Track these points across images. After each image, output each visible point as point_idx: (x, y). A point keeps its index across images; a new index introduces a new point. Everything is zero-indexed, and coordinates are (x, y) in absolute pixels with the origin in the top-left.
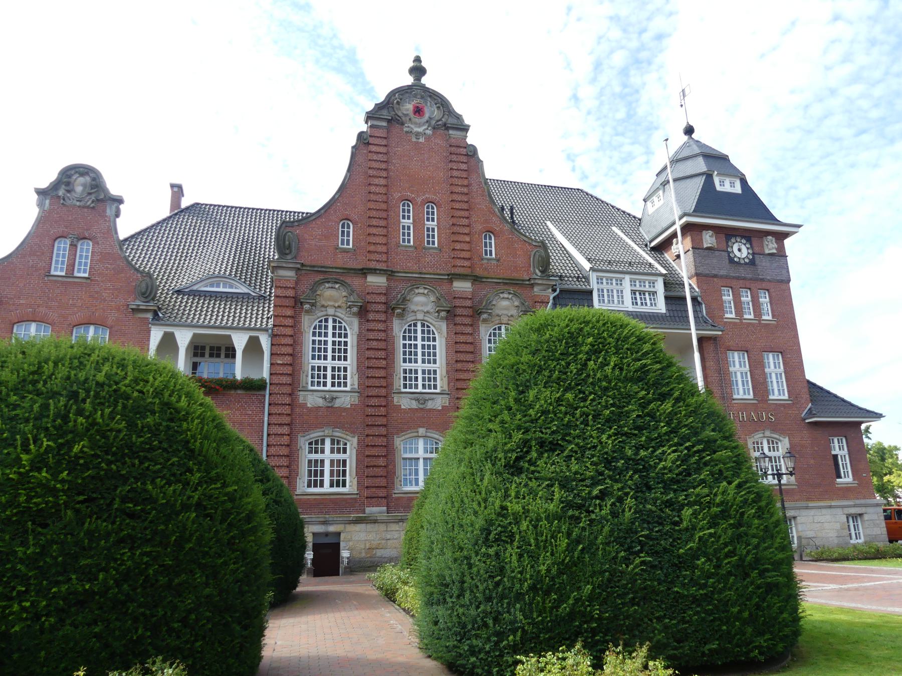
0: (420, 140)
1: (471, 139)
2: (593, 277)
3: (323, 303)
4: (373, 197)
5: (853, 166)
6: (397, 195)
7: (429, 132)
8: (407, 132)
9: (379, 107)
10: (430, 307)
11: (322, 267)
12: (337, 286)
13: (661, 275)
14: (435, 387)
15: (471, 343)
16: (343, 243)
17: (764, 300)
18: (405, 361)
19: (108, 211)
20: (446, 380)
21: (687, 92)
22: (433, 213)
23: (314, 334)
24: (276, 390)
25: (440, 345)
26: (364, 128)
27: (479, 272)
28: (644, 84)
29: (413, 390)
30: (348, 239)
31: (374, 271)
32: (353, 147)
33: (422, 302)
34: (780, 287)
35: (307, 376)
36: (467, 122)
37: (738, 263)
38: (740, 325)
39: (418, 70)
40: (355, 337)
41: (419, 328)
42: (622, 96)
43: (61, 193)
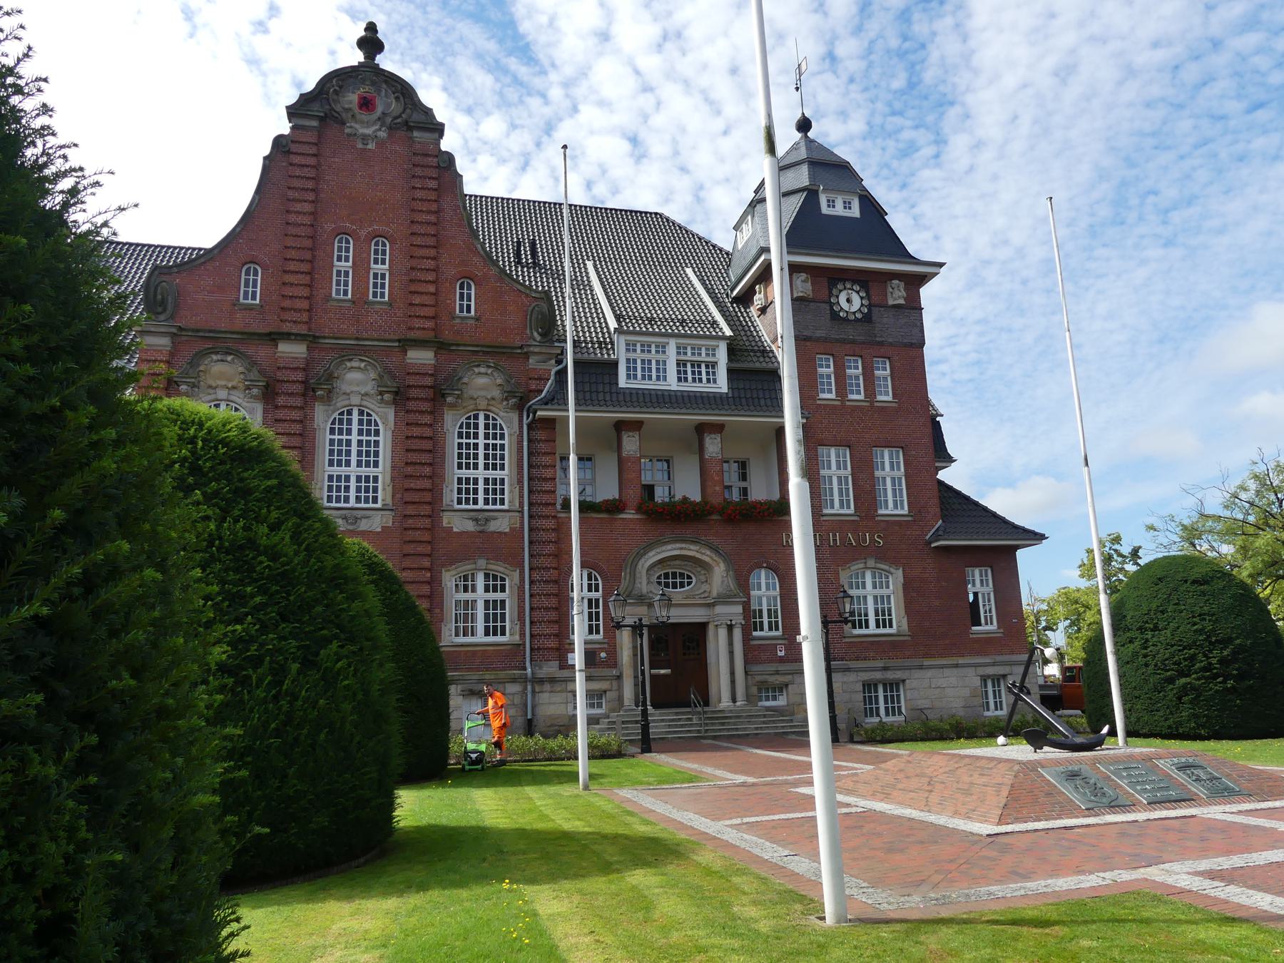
0: (370, 147)
1: (446, 145)
2: (620, 342)
5: (1241, 159)
7: (383, 134)
8: (349, 135)
9: (305, 100)
10: (370, 387)
11: (210, 331)
12: (229, 358)
13: (724, 338)
14: (375, 500)
15: (431, 438)
16: (246, 298)
17: (883, 372)
18: (460, 467)
20: (389, 489)
22: (384, 253)
23: (332, 431)
25: (385, 441)
26: (285, 128)
27: (447, 335)
28: (934, 33)
29: (342, 505)
30: (252, 289)
31: (287, 336)
32: (265, 158)
33: (357, 380)
35: (321, 489)
37: (846, 320)
39: (371, 43)
42: (901, 54)
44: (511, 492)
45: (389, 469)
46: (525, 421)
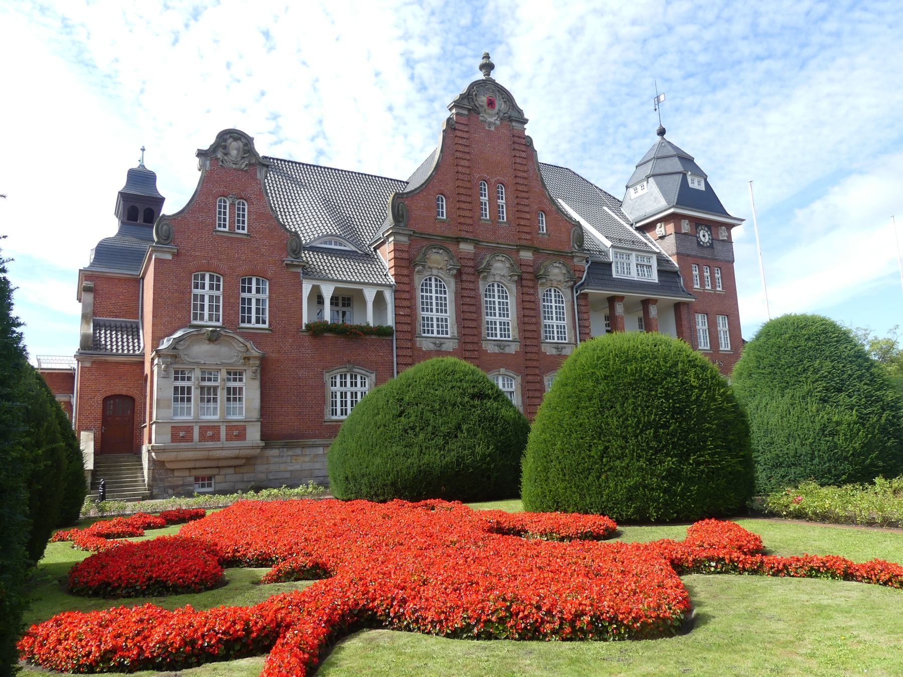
3: (430, 265)
4: (461, 176)
6: (477, 176)
7: (498, 122)
9: (463, 97)
10: (505, 272)
12: (441, 251)
13: (655, 253)
14: (447, 334)
19: (258, 174)
21: (662, 98)
24: (401, 336)
25: (450, 296)
31: (465, 240)
32: (444, 131)
33: (500, 267)
34: (726, 265)
36: (526, 116)
38: (703, 294)
40: (453, 295)
41: (496, 288)
43: (219, 155)
44: (569, 333)
45: (515, 319)
46: (575, 295)
